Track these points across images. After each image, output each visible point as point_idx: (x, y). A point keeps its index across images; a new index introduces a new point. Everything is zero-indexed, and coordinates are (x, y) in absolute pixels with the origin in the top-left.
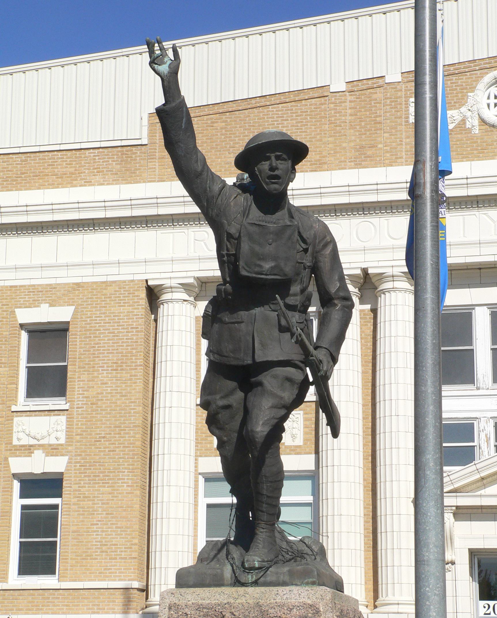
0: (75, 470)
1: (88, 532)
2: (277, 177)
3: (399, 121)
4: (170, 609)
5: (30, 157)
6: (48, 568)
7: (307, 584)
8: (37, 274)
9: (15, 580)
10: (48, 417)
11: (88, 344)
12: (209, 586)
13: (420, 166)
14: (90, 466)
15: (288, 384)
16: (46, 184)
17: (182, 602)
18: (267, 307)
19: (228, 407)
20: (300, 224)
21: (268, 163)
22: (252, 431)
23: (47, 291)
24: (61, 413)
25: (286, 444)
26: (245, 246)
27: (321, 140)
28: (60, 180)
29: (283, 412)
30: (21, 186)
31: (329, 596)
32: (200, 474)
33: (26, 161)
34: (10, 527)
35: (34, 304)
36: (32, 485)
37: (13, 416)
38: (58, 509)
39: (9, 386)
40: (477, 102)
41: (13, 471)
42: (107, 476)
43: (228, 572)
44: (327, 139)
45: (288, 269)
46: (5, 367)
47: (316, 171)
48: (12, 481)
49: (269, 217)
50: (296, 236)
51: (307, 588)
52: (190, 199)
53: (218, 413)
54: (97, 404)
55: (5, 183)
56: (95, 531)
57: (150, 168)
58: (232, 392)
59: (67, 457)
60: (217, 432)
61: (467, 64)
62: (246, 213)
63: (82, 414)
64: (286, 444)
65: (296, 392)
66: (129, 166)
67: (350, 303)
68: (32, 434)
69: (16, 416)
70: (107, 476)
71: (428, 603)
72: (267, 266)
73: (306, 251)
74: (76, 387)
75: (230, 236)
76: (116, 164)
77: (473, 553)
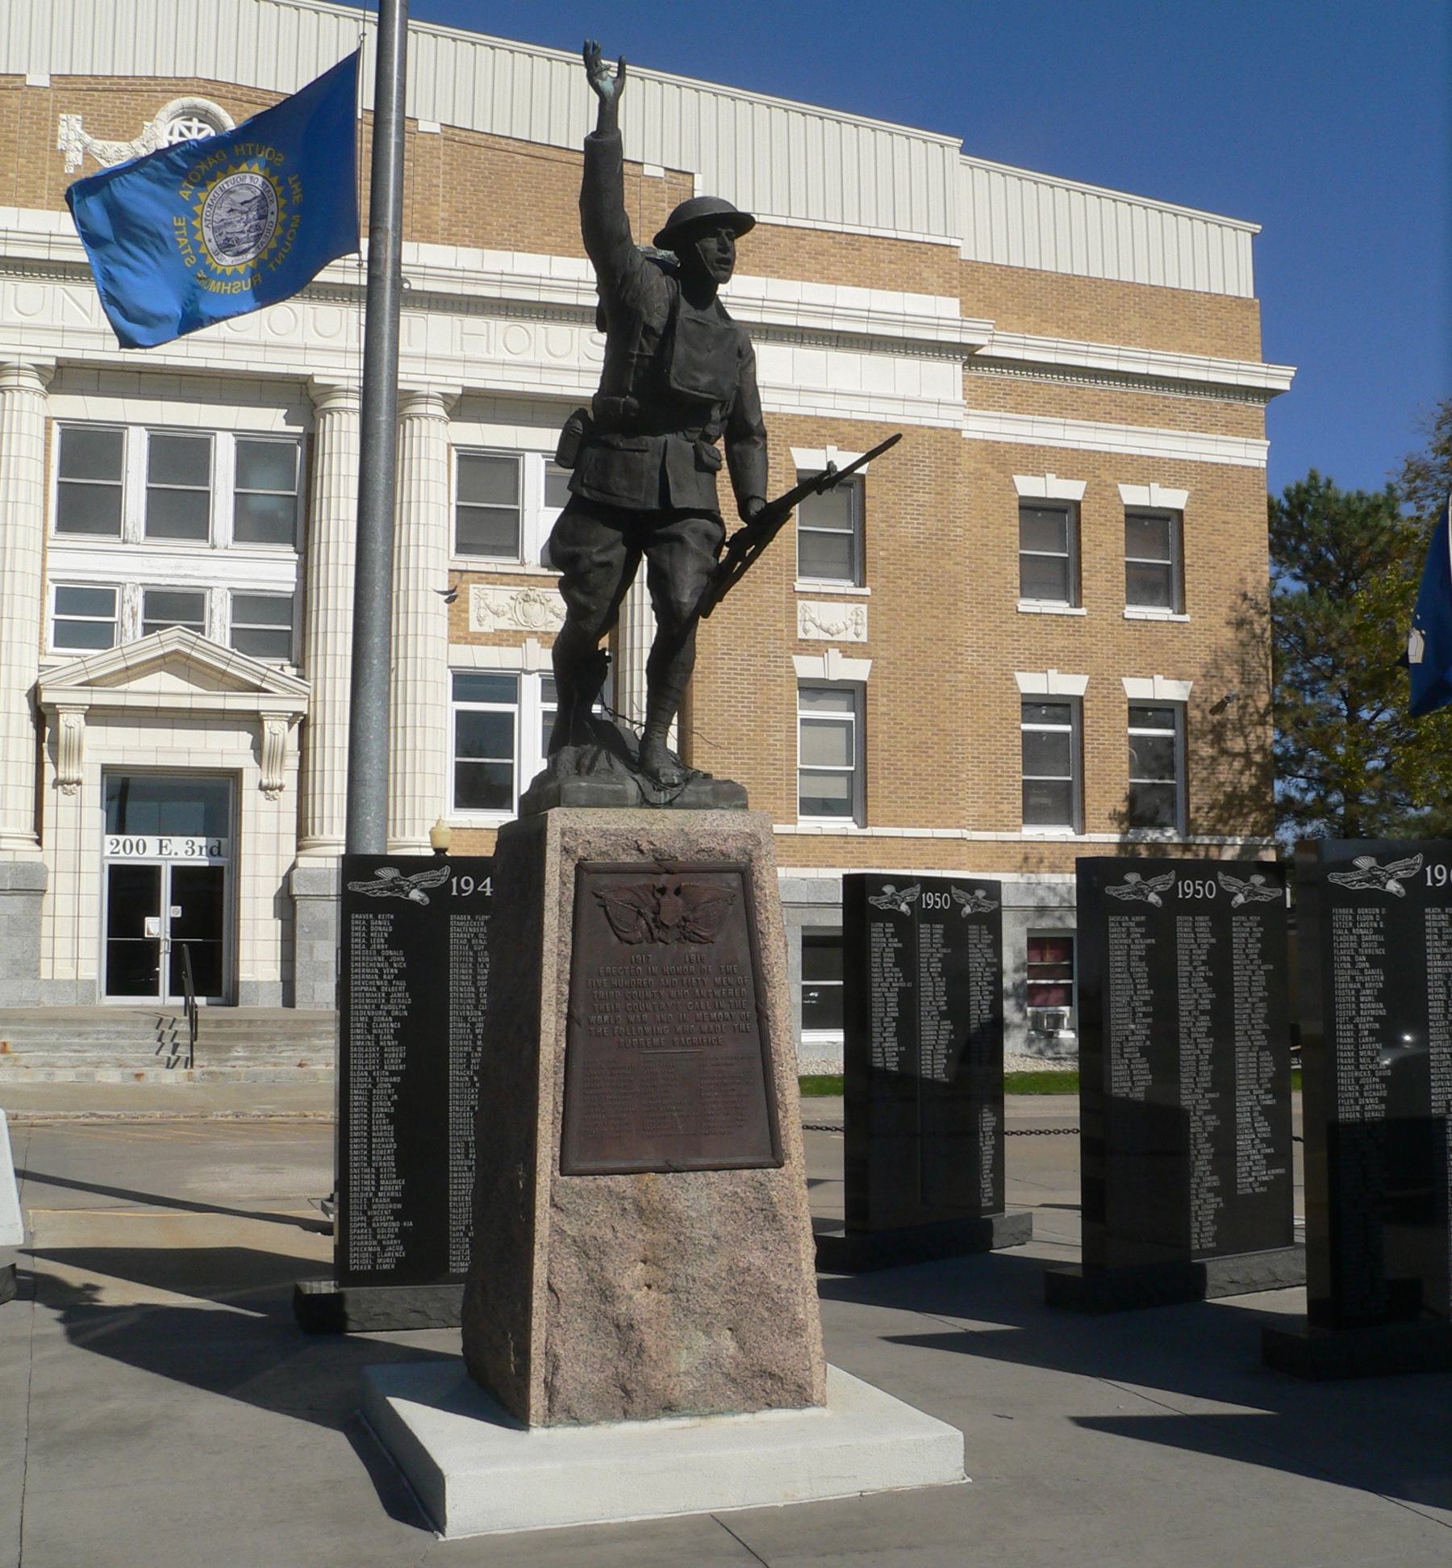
3: (41, 143)
4: (563, 834)
12: (607, 806)
13: (379, 236)
18: (681, 434)
35: (1143, 480)
40: (157, 137)
52: (79, 241)
61: (145, 81)
72: (704, 379)
77: (107, 770)
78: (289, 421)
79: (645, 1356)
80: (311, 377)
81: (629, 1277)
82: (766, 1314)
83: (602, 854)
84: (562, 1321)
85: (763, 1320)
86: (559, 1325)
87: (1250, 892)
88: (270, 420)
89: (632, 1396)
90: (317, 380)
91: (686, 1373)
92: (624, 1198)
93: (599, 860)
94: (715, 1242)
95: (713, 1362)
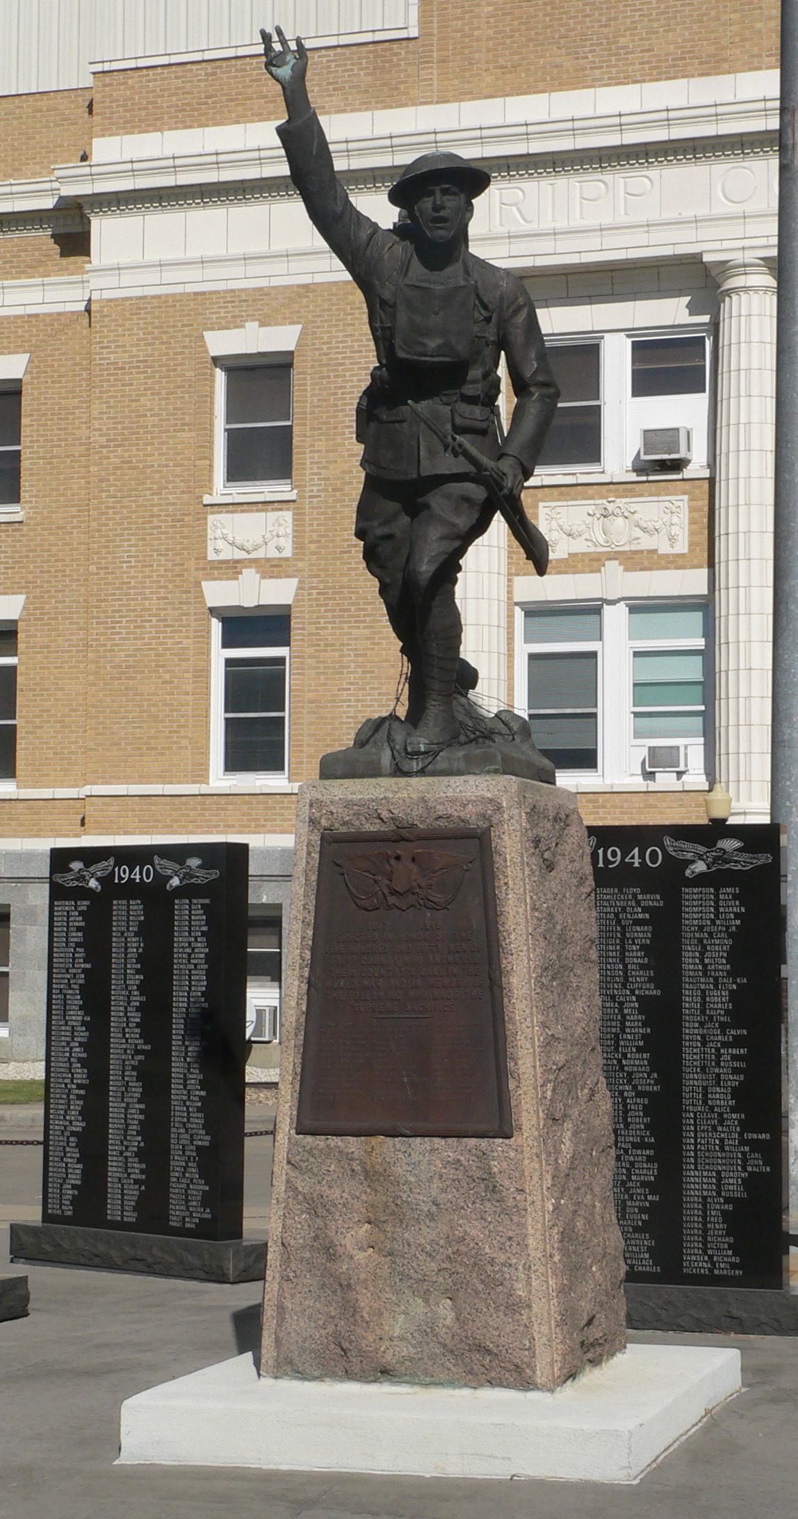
0: (310, 600)
1: (334, 701)
2: (443, 220)
4: (311, 805)
5: (221, 67)
6: (272, 760)
7: (488, 772)
8: (237, 270)
9: (220, 780)
10: (263, 514)
11: (325, 389)
14: (334, 593)
15: (465, 505)
16: (249, 113)
17: (327, 798)
18: (437, 399)
19: (389, 537)
20: (479, 284)
21: (431, 199)
22: (414, 570)
23: (255, 300)
24: (285, 506)
25: (660, 552)
26: (402, 318)
27: (717, 19)
28: (272, 105)
29: (457, 544)
30: (207, 119)
31: (515, 788)
32: (516, 604)
33: (214, 74)
34: (208, 694)
35: (234, 322)
36: (242, 626)
37: (206, 513)
38: (284, 664)
39: (197, 463)
41: (209, 605)
42: (363, 610)
43: (386, 759)
44: (727, 16)
45: (462, 348)
46: (190, 430)
47: (708, 74)
48: (209, 620)
49: (437, 276)
50: (473, 300)
51: (488, 778)
53: (376, 546)
54: (342, 490)
55: (180, 115)
56: (345, 701)
57: (425, 80)
58: (395, 516)
59: (296, 580)
60: (377, 570)
62: (405, 269)
63: (319, 507)
64: (660, 552)
65: (476, 515)
66: (387, 77)
67: (552, 390)
68: (238, 542)
69: (212, 513)
70: (363, 610)
71: (788, 804)
72: (433, 343)
73: (488, 320)
74: (308, 462)
75: (383, 303)
76: (365, 75)
78: (693, 309)
79: (358, 1317)
80: (701, 254)
81: (353, 1238)
82: (480, 1287)
83: (345, 823)
84: (292, 1275)
85: (477, 1292)
86: (289, 1280)
87: (716, 859)
88: (669, 313)
89: (348, 1357)
90: (706, 258)
91: (402, 1338)
92: (352, 1159)
93: (343, 829)
94: (434, 1208)
95: (428, 1330)
